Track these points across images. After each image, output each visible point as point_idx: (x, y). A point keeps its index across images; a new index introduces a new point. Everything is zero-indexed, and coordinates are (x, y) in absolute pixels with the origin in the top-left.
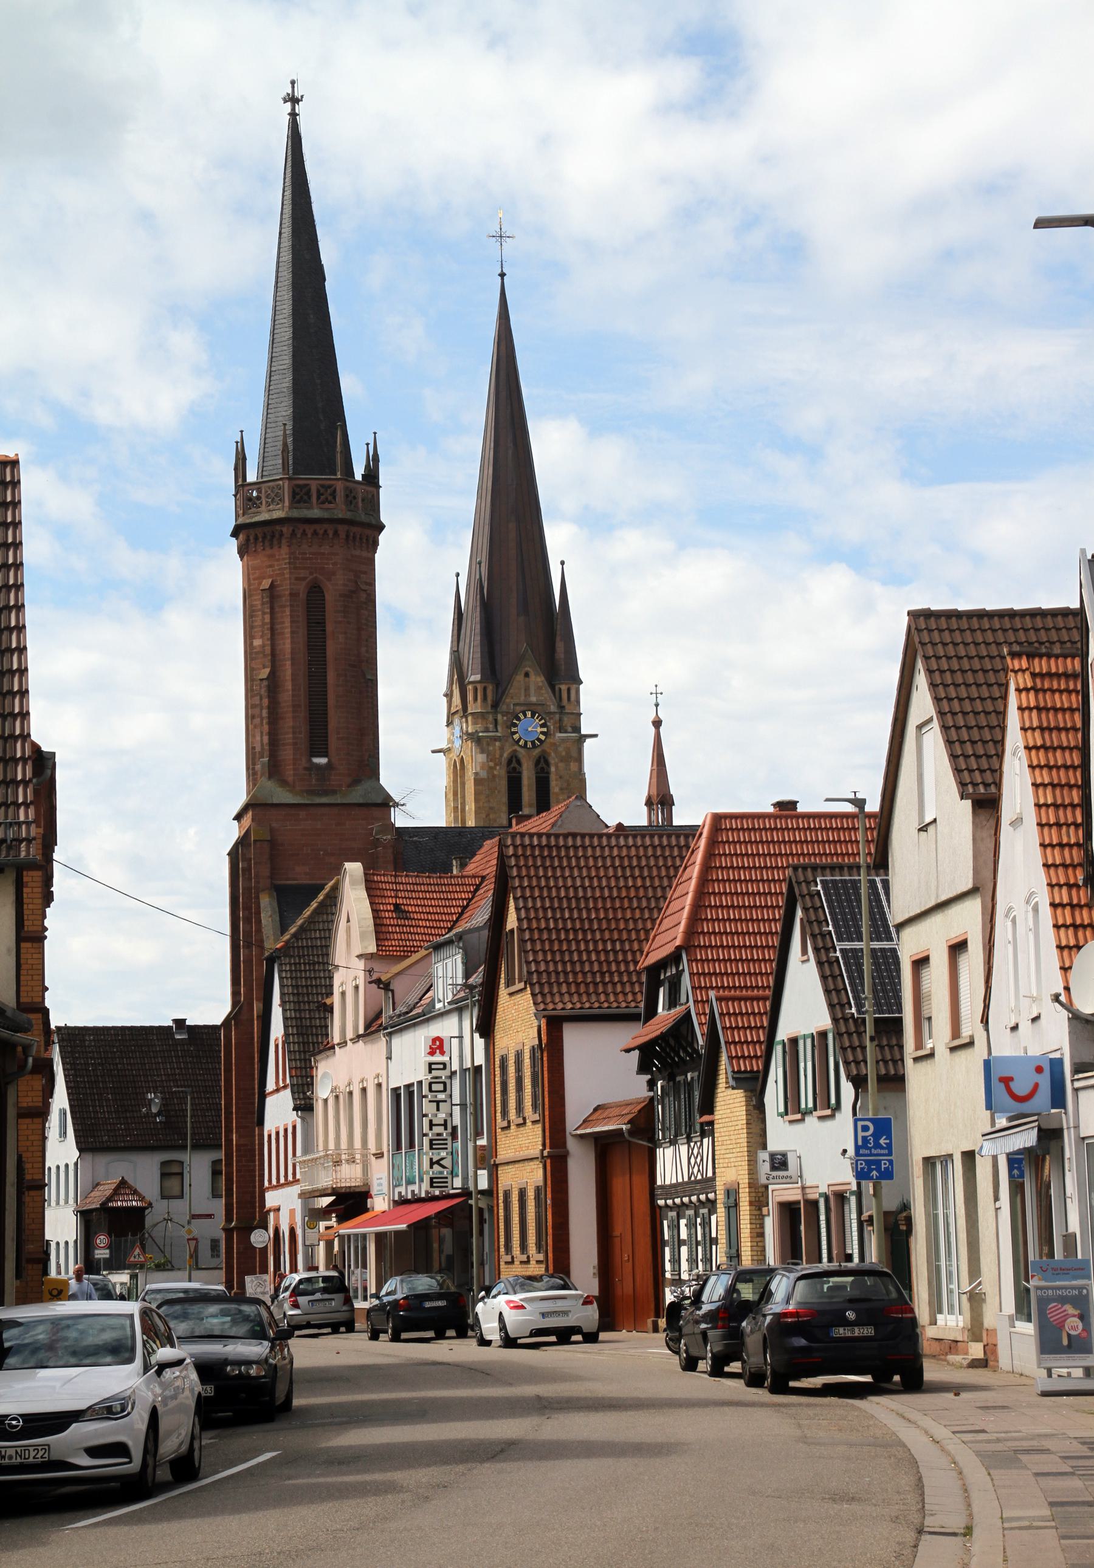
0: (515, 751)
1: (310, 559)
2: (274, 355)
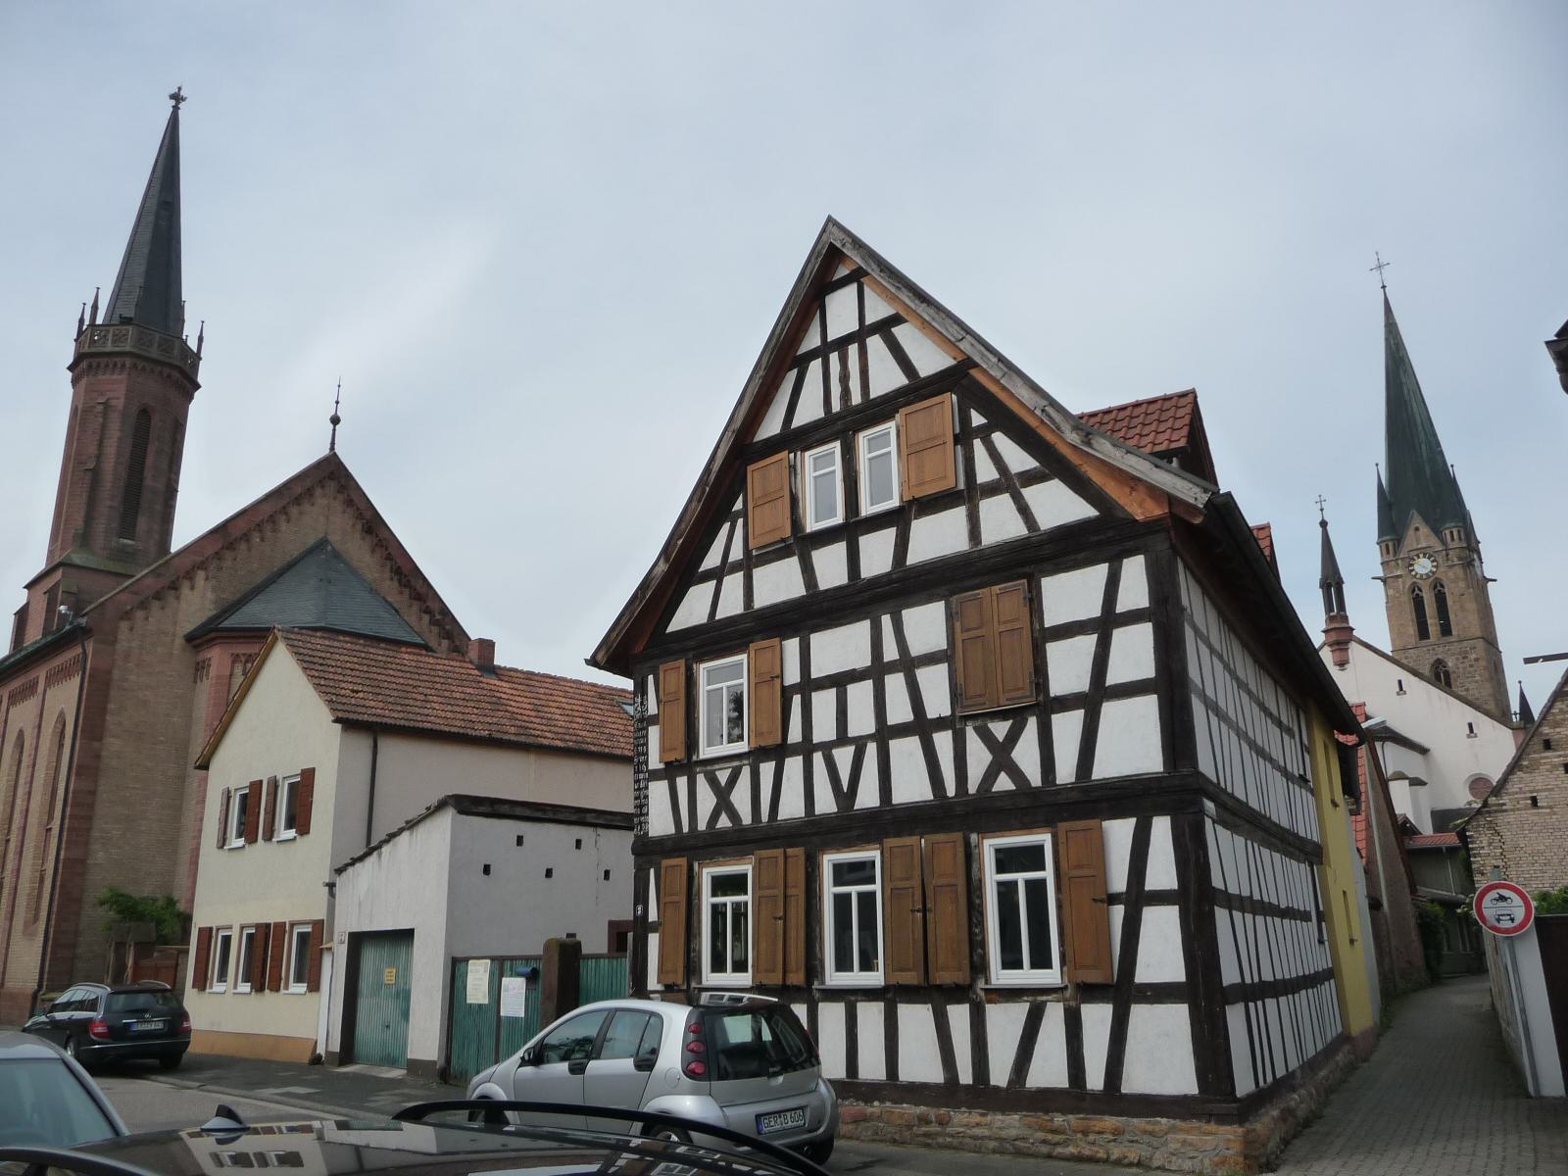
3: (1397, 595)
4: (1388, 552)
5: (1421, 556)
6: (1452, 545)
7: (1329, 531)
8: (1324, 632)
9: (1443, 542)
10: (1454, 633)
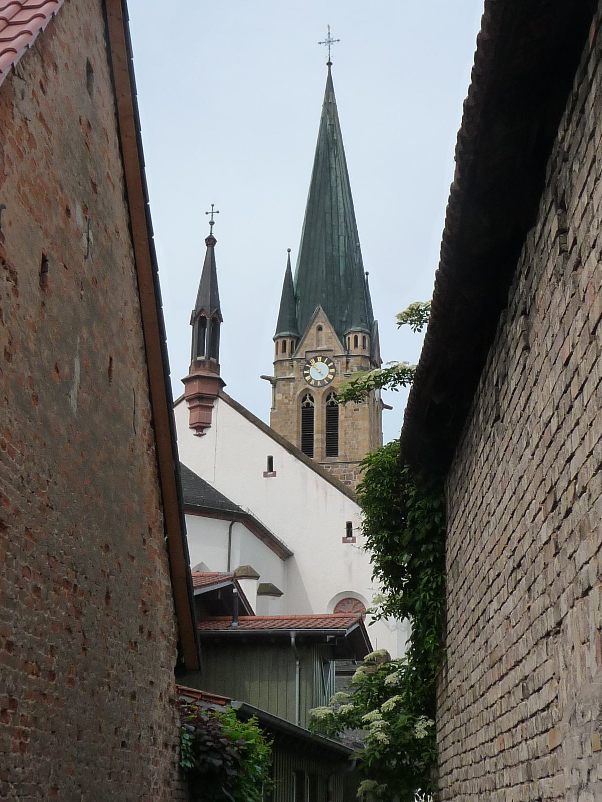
0: (307, 389)
3: (286, 401)
4: (284, 350)
5: (320, 359)
6: (354, 352)
7: (215, 250)
9: (346, 347)
10: (339, 454)
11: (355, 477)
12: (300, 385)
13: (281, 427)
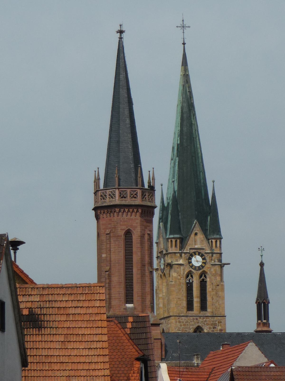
0: (191, 271)
1: (126, 221)
2: (112, 136)
3: (179, 277)
8: (119, 38)
10: (209, 310)
11: (218, 324)
12: (186, 269)
13: (177, 293)
